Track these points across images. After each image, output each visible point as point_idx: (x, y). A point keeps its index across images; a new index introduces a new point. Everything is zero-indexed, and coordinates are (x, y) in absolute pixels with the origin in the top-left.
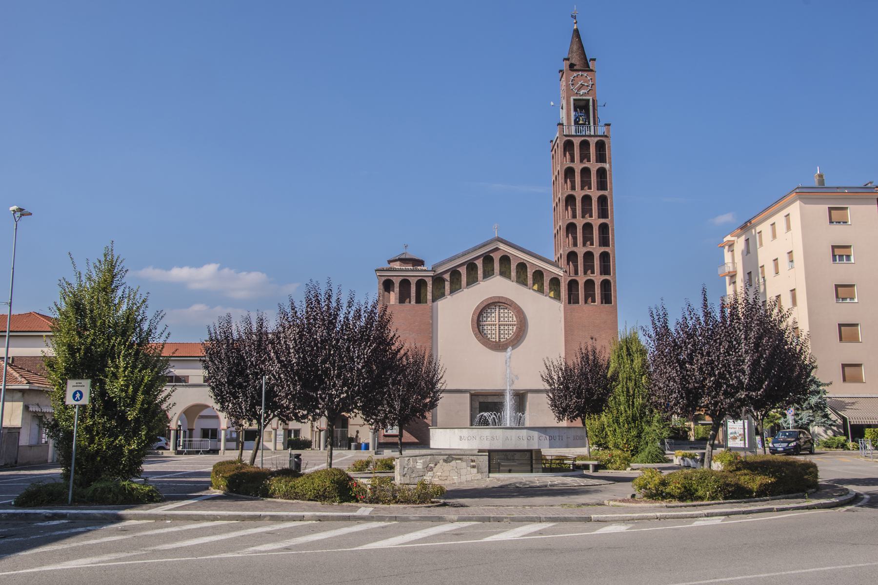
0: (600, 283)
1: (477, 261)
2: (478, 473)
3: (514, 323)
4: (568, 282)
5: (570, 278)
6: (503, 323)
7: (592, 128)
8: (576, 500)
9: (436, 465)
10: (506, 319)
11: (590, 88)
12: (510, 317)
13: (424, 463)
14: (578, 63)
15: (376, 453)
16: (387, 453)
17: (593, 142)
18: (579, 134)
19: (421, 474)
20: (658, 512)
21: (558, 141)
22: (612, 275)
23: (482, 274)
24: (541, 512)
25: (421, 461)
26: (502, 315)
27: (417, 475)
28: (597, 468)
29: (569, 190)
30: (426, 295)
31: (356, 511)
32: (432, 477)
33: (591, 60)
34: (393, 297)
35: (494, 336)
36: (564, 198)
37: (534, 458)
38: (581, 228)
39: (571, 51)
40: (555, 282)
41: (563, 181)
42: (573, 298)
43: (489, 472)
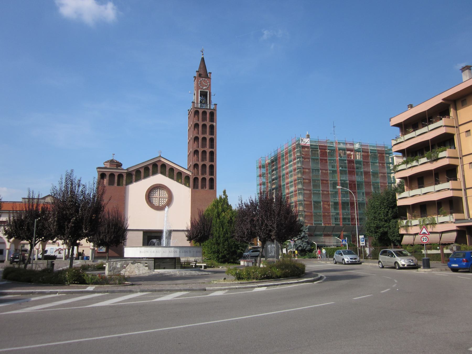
0: (209, 179)
1: (150, 166)
2: (148, 269)
3: (166, 197)
4: (193, 178)
5: (195, 177)
6: (161, 197)
7: (208, 105)
8: (198, 281)
9: (127, 265)
10: (163, 195)
11: (208, 86)
12: (164, 194)
13: (121, 265)
14: (203, 74)
15: (93, 262)
16: (99, 261)
17: (208, 112)
18: (202, 108)
19: (119, 270)
20: (237, 285)
21: (192, 110)
22: (214, 176)
23: (152, 172)
24: (181, 287)
25: (120, 264)
26: (161, 193)
27: (117, 271)
28: (205, 267)
29: (196, 134)
30: (123, 182)
31: (86, 288)
32: (125, 271)
33: (209, 73)
34: (106, 181)
35: (156, 203)
36: (193, 138)
37: (176, 262)
38: (201, 152)
39: (200, 68)
40: (187, 177)
41: (193, 130)
42: (195, 186)
43: (154, 269)
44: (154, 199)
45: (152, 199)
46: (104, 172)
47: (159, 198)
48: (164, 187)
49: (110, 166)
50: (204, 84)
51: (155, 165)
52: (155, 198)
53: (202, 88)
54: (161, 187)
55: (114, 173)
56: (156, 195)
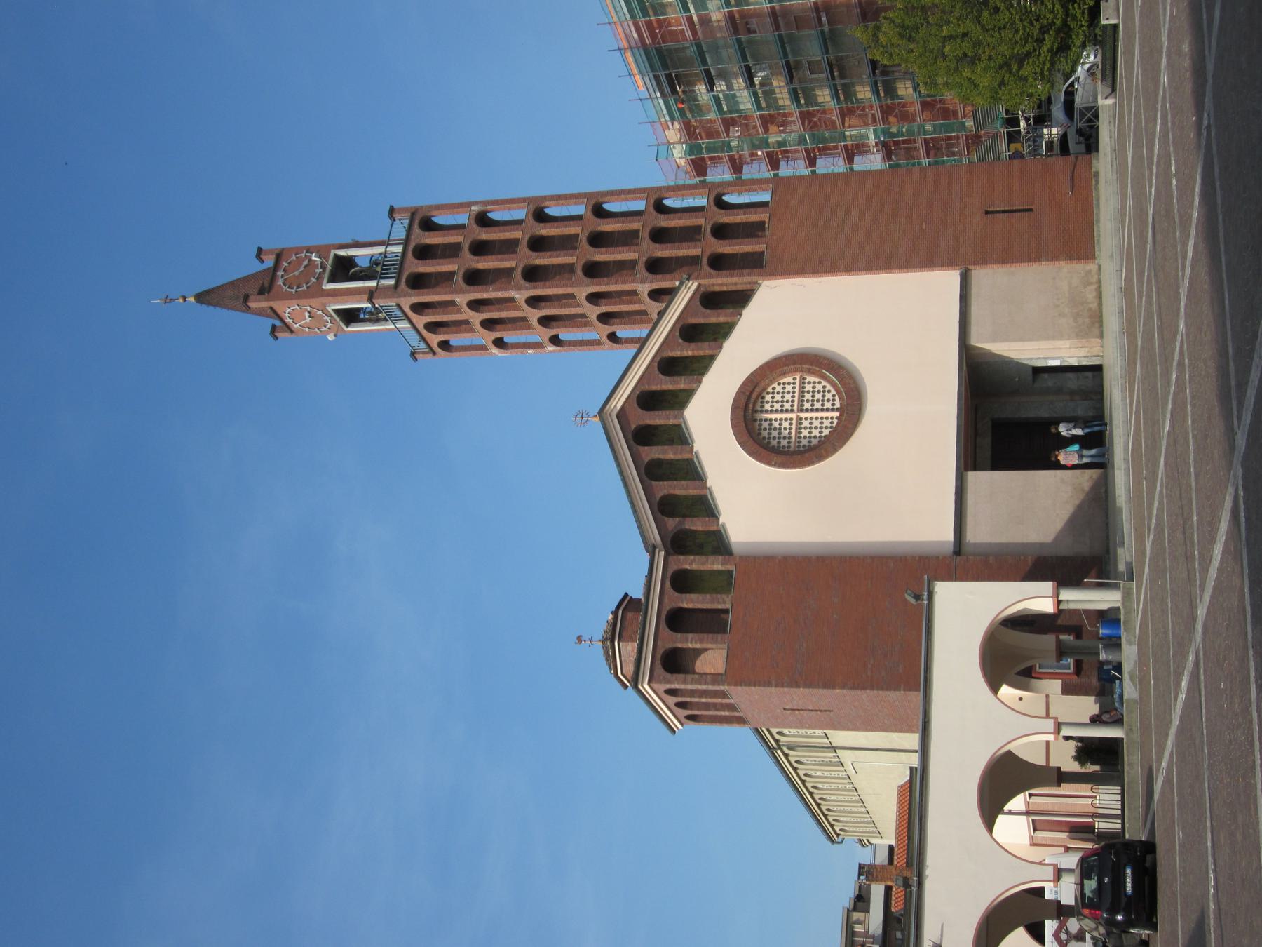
26: (777, 406)
35: (827, 423)
42: (755, 263)
44: (805, 433)
45: (804, 442)
46: (659, 656)
47: (802, 411)
48: (750, 389)
49: (633, 641)
50: (302, 269)
51: (642, 437)
52: (799, 428)
53: (317, 279)
54: (747, 404)
55: (667, 608)
56: (786, 424)
